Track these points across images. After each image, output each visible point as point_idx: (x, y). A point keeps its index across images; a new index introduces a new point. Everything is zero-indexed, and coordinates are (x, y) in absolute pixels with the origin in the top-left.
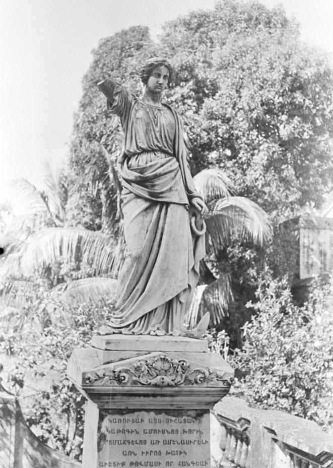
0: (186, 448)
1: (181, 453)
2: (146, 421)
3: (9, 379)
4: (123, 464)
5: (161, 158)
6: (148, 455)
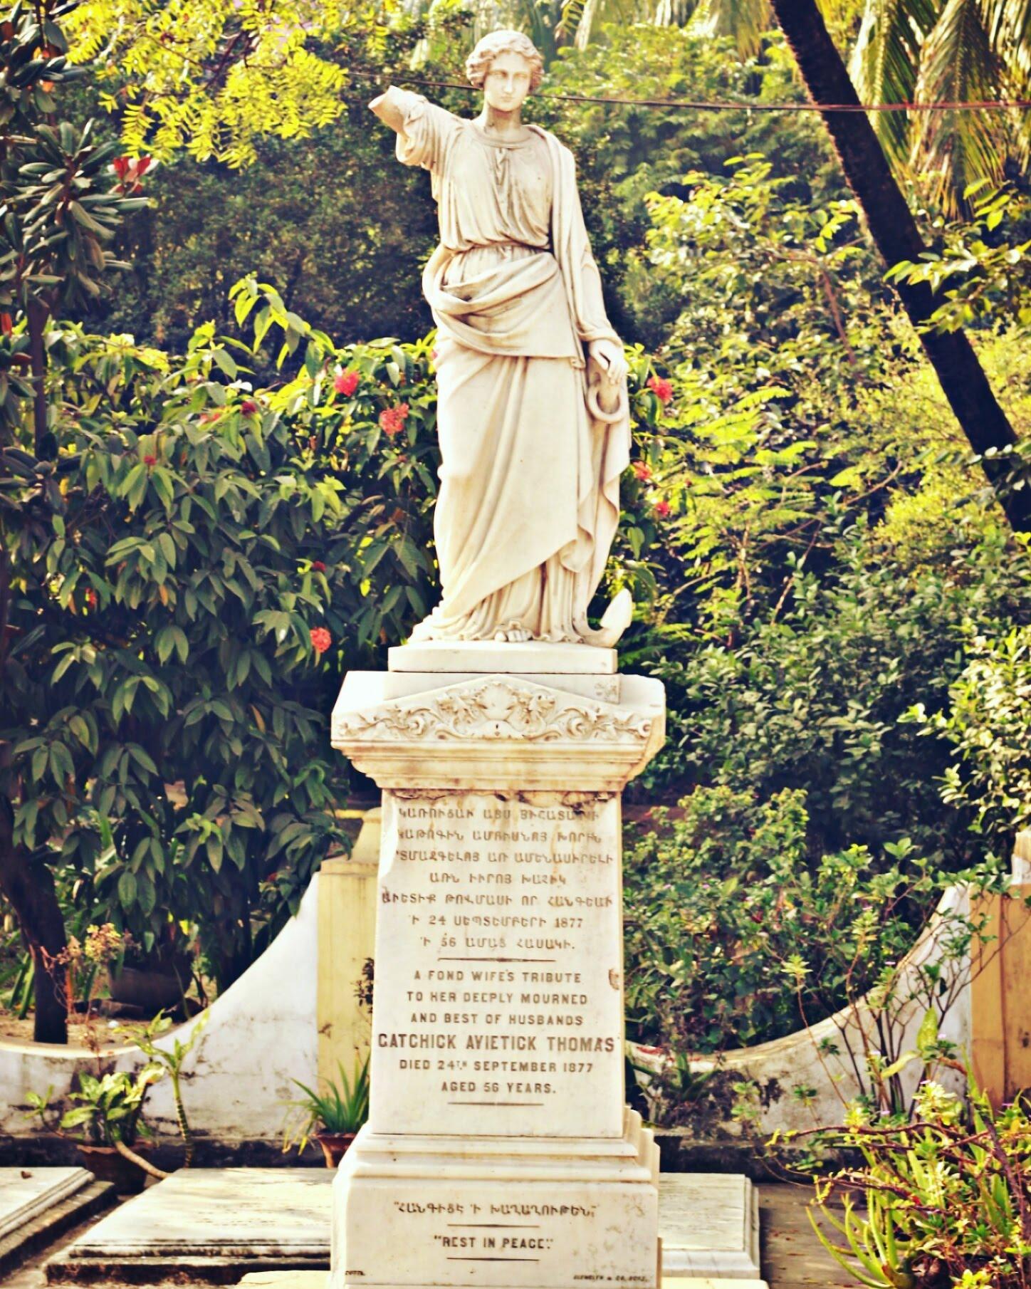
0: (564, 869)
1: (553, 879)
2: (478, 814)
4: (431, 898)
6: (484, 882)
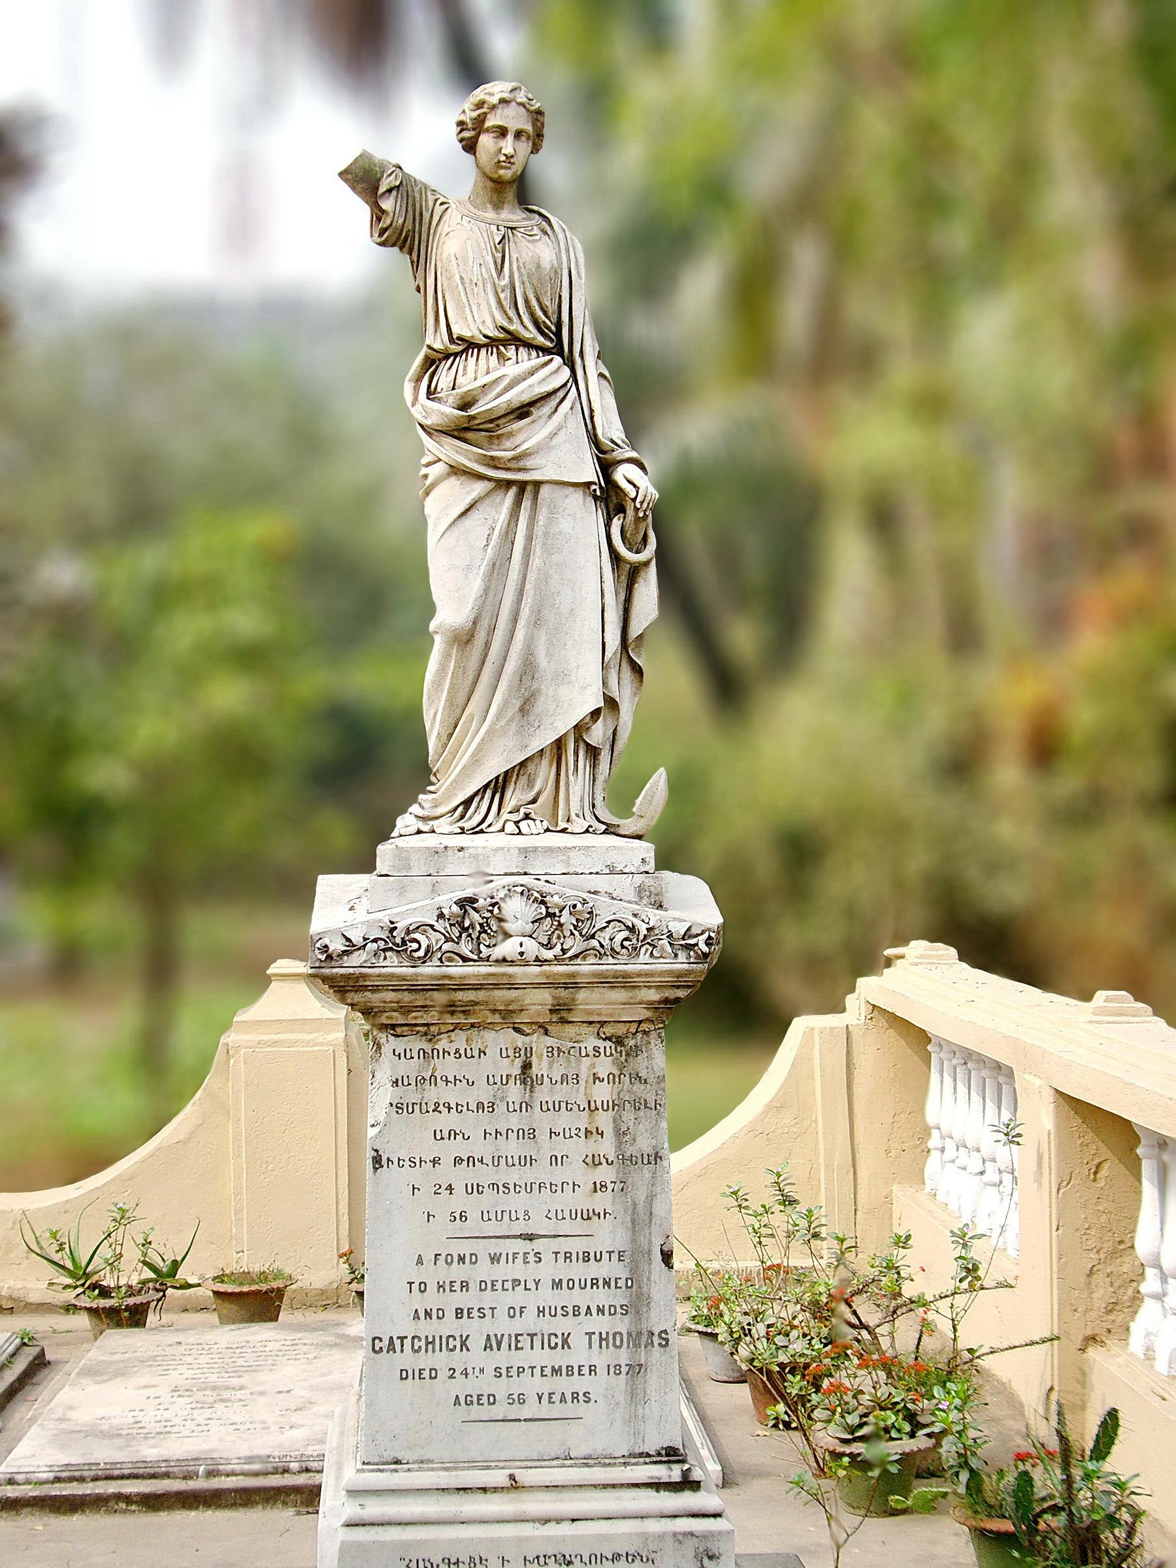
3: (706, 1334)
4: (435, 1162)
5: (521, 362)
